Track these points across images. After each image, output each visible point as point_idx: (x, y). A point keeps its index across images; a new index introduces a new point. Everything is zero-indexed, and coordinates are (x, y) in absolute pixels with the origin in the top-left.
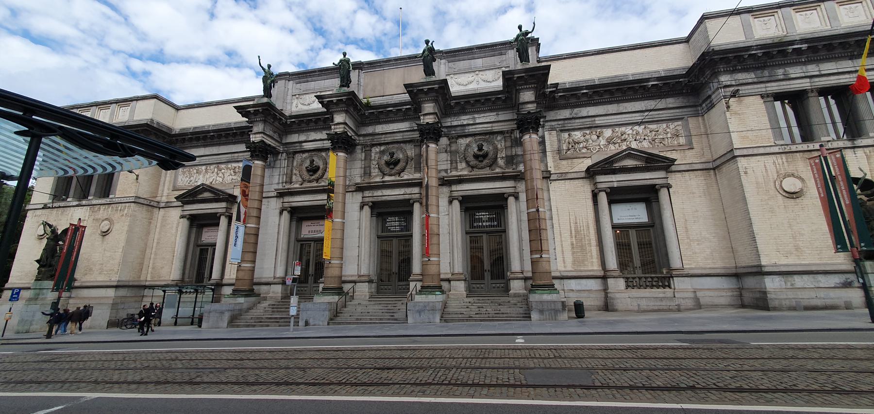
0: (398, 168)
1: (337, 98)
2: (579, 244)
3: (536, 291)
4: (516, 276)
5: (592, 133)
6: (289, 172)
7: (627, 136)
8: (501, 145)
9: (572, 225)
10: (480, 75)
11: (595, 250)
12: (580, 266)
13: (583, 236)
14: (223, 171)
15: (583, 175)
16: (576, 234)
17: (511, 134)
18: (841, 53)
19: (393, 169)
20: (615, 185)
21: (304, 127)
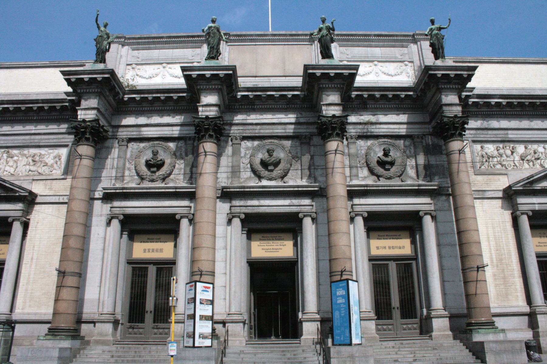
3: (479, 330)
4: (438, 313)
5: (506, 147)
6: (121, 164)
7: (540, 155)
8: (410, 151)
10: (167, 69)
12: (504, 300)
14: (15, 158)
15: (500, 194)
20: (537, 207)
21: (145, 107)
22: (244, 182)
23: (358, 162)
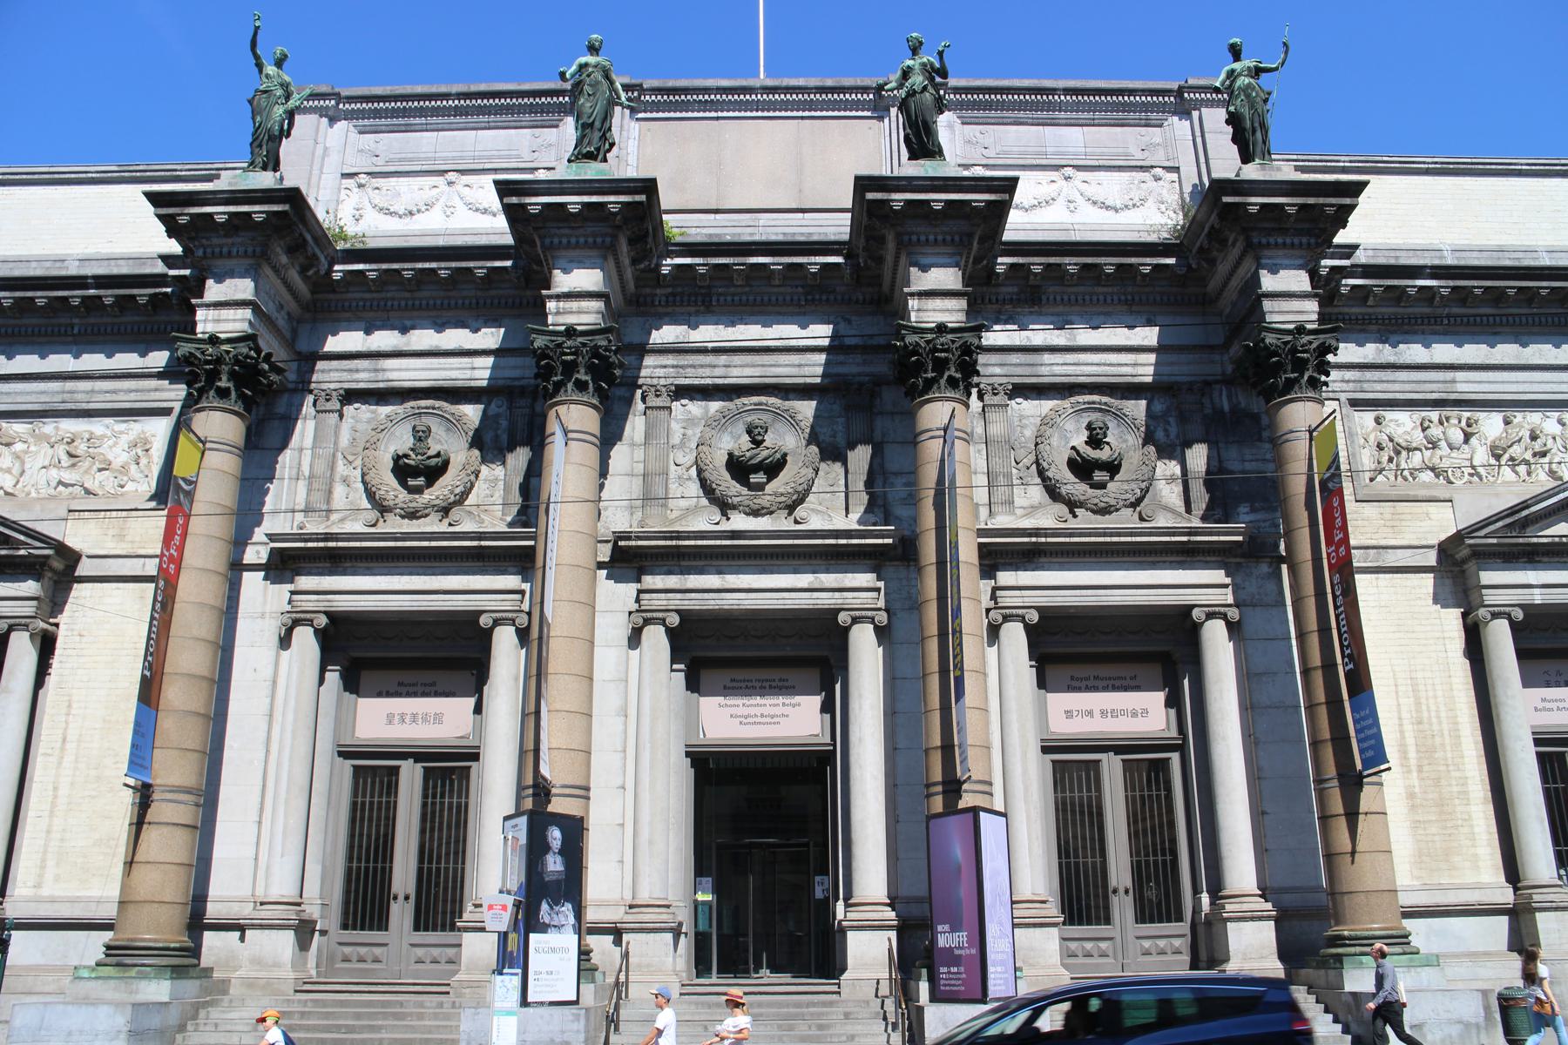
0: (780, 485)
1: (586, 199)
2: (1431, 796)
4: (1245, 907)
6: (321, 468)
7: (1550, 442)
8: (1166, 430)
9: (1408, 728)
11: (1482, 815)
13: (1443, 768)
14: (19, 447)
16: (1419, 759)
17: (1203, 395)
18: (594, 235)
19: (418, 490)
22: (679, 519)
23: (1013, 463)
